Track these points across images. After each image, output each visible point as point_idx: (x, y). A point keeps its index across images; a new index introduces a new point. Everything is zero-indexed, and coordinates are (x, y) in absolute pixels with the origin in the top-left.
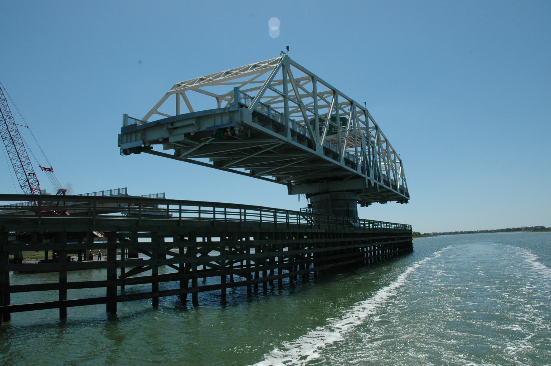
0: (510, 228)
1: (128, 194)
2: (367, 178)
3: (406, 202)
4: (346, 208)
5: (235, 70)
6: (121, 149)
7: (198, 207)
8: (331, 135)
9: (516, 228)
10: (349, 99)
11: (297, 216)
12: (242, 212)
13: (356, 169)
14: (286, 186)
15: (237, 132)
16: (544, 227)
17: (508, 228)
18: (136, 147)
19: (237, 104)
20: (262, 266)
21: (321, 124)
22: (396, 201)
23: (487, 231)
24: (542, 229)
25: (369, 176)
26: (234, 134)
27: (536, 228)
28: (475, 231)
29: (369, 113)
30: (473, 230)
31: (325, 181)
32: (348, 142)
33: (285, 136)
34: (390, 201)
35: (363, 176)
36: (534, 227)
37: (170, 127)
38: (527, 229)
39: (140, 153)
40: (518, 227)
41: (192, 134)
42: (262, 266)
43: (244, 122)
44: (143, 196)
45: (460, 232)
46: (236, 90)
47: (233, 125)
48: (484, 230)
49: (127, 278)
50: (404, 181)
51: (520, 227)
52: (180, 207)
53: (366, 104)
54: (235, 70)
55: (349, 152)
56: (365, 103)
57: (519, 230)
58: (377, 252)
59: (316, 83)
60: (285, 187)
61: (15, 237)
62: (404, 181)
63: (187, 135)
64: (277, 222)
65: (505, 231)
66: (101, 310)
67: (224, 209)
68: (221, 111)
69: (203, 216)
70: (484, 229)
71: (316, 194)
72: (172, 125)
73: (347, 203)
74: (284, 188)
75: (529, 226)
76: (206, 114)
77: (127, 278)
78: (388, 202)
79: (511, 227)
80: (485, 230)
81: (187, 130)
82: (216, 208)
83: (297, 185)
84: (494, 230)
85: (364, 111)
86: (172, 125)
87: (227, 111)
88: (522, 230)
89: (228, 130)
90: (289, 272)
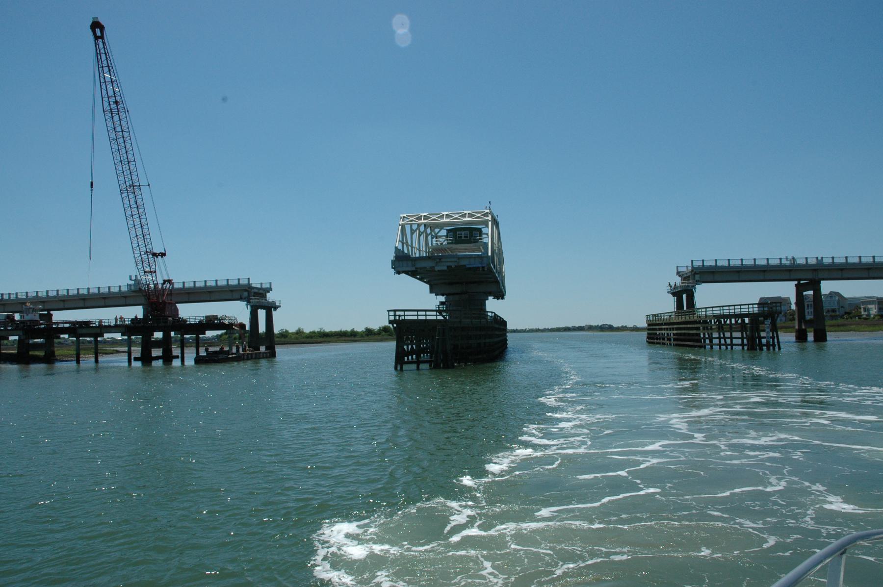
0: (569, 326)
3: (503, 298)
9: (577, 326)
11: (720, 335)
12: (726, 336)
15: (486, 269)
16: (612, 326)
17: (567, 326)
22: (493, 297)
23: (538, 330)
24: (610, 328)
26: (484, 270)
27: (602, 326)
28: (523, 330)
30: (519, 329)
36: (600, 325)
37: (438, 260)
38: (590, 328)
40: (580, 325)
45: (551, 329)
47: (483, 266)
48: (534, 328)
50: (405, 245)
51: (582, 326)
56: (490, 202)
57: (581, 329)
62: (405, 245)
66: (414, 366)
69: (428, 318)
70: (534, 327)
72: (440, 259)
75: (594, 324)
79: (570, 325)
80: (536, 329)
81: (449, 264)
84: (548, 329)
88: (584, 329)
89: (481, 268)
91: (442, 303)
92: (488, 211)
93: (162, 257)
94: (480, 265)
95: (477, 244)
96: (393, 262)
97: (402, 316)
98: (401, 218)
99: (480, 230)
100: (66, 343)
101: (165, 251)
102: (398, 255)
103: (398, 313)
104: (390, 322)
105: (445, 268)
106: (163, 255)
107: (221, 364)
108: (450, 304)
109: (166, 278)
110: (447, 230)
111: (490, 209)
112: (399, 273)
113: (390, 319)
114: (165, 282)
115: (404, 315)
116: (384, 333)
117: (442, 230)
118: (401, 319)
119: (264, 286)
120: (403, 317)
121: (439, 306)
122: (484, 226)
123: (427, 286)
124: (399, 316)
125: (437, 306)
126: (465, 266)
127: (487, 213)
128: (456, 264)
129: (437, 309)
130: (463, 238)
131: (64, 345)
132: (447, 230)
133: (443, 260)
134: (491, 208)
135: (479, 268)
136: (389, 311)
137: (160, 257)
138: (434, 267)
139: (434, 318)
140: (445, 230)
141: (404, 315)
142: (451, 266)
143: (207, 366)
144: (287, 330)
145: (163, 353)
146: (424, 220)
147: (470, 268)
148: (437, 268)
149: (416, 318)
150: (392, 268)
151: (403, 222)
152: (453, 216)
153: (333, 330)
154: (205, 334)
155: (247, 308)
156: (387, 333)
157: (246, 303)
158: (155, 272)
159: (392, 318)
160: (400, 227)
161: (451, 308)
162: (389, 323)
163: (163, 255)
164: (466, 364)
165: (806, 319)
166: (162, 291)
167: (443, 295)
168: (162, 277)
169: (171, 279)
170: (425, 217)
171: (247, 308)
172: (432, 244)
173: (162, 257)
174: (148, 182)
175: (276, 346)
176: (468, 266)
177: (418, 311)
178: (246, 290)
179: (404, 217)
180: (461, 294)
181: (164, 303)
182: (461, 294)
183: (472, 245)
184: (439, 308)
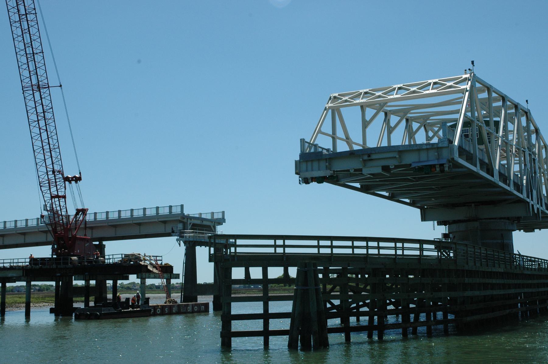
1: (184, 214)
2: (532, 203)
4: (500, 241)
6: (299, 177)
7: (376, 243)
10: (514, 103)
13: (520, 192)
14: (418, 211)
15: (446, 169)
18: (321, 177)
19: (446, 140)
21: (468, 130)
25: (532, 200)
26: (442, 171)
29: (531, 115)
31: (473, 205)
32: (501, 153)
33: (474, 166)
34: (540, 229)
35: (528, 200)
37: (366, 157)
39: (323, 183)
43: (455, 159)
44: (189, 215)
46: (445, 125)
47: (442, 162)
52: (396, 245)
53: (528, 103)
56: (527, 101)
58: (412, 316)
59: (492, 94)
60: (418, 211)
61: (22, 271)
63: (385, 168)
67: (377, 243)
68: (428, 147)
69: (382, 252)
71: (455, 222)
72: (369, 156)
73: (502, 235)
74: (417, 212)
76: (411, 149)
78: (535, 230)
82: (397, 244)
83: (430, 208)
85: (526, 113)
86: (369, 156)
87: (435, 146)
90: (455, 317)
93: (76, 182)
94: (435, 162)
98: (330, 99)
100: (134, 288)
101: (80, 173)
106: (77, 179)
107: (108, 320)
109: (80, 207)
112: (306, 181)
114: (78, 211)
119: (216, 217)
131: (132, 290)
133: (374, 157)
134: (527, 103)
135: (434, 166)
137: (73, 182)
138: (361, 170)
143: (154, 318)
145: (55, 305)
149: (315, 251)
150: (297, 173)
152: (409, 90)
154: (127, 278)
155: (180, 244)
157: (176, 237)
158: (64, 197)
163: (77, 179)
166: (83, 223)
168: (75, 204)
169: (86, 208)
171: (180, 244)
173: (76, 182)
174: (60, 83)
175: (112, 298)
177: (353, 239)
178: (180, 222)
179: (335, 97)
181: (74, 238)
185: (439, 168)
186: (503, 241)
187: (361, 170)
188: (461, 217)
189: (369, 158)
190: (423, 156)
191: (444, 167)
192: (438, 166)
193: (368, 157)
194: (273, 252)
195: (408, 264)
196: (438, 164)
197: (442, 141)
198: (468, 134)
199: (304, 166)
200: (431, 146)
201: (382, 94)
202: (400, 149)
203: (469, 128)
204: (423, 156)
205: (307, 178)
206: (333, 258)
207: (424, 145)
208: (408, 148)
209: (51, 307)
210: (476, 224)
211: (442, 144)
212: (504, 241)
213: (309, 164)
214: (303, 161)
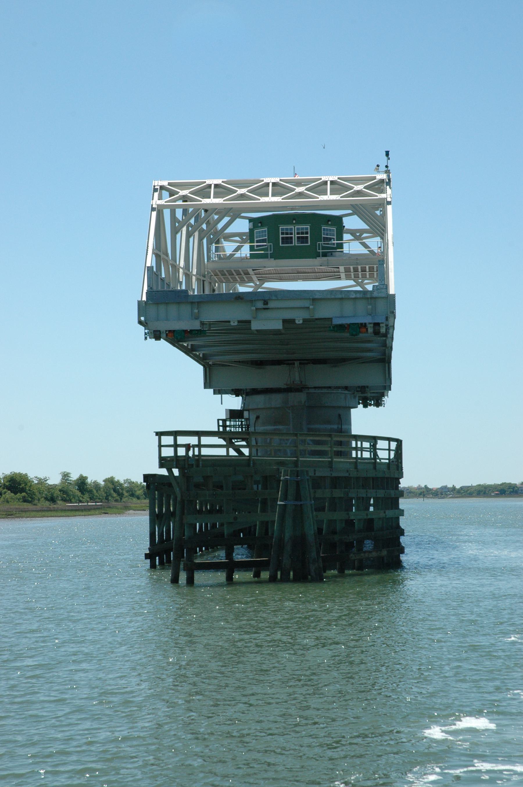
0: (513, 482)
5: (299, 183)
8: (313, 258)
20: (242, 536)
21: (291, 229)
37: (260, 305)
41: (297, 322)
42: (242, 536)
45: (462, 488)
48: (415, 486)
49: (157, 539)
54: (299, 183)
55: (148, 267)
56: (387, 153)
64: (372, 457)
65: (497, 496)
66: (221, 576)
71: (255, 392)
72: (266, 303)
73: (339, 415)
76: (333, 297)
77: (157, 539)
80: (419, 488)
81: (288, 315)
84: (454, 488)
86: (266, 303)
87: (369, 296)
91: (233, 414)
92: (384, 176)
94: (367, 320)
95: (329, 258)
96: (142, 308)
97: (194, 446)
98: (155, 190)
99: (338, 221)
102: (155, 289)
103: (181, 440)
104: (163, 462)
105: (278, 326)
108: (258, 418)
110: (251, 220)
111: (388, 172)
112: (157, 335)
113: (163, 455)
115: (199, 446)
116: (9, 494)
117: (238, 220)
118: (191, 454)
120: (196, 450)
121: (224, 421)
122: (350, 212)
123: (198, 369)
124: (188, 447)
125: (221, 423)
126: (330, 319)
127: (382, 181)
128: (306, 315)
129: (221, 429)
130: (295, 243)
132: (251, 220)
133: (271, 304)
135: (364, 326)
136: (160, 434)
138: (249, 322)
139: (222, 452)
140: (247, 221)
141: (199, 446)
142: (292, 321)
144: (104, 479)
146: (214, 198)
147: (341, 327)
148: (255, 326)
150: (140, 322)
151: (160, 202)
153: (512, 483)
156: (19, 495)
159: (168, 452)
160: (154, 214)
161: (260, 428)
162: (161, 466)
164: (341, 571)
165: (195, 571)
167: (237, 393)
170: (218, 190)
172: (209, 258)
176: (337, 322)
179: (162, 188)
180: (288, 390)
182: (288, 390)
183: (319, 260)
184: (225, 426)
185: (372, 329)
186: (341, 427)
187: (249, 322)
188: (280, 384)
189: (266, 306)
190: (348, 308)
191: (380, 326)
192: (372, 325)
193: (264, 304)
194: (225, 454)
195: (367, 471)
196: (370, 323)
197: (379, 289)
198: (292, 237)
199: (152, 310)
200: (362, 295)
201: (247, 192)
202: (317, 297)
203: (295, 227)
204: (348, 308)
205: (160, 331)
206: (299, 463)
207: (352, 293)
208: (329, 297)
209: (404, 517)
210: (302, 397)
211: (378, 293)
212: (343, 427)
213: (162, 308)
214: (154, 303)
